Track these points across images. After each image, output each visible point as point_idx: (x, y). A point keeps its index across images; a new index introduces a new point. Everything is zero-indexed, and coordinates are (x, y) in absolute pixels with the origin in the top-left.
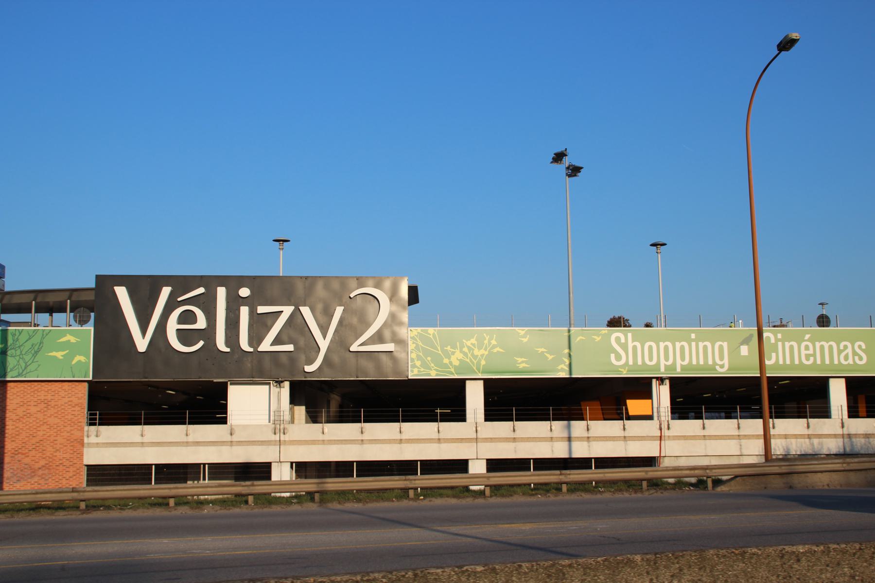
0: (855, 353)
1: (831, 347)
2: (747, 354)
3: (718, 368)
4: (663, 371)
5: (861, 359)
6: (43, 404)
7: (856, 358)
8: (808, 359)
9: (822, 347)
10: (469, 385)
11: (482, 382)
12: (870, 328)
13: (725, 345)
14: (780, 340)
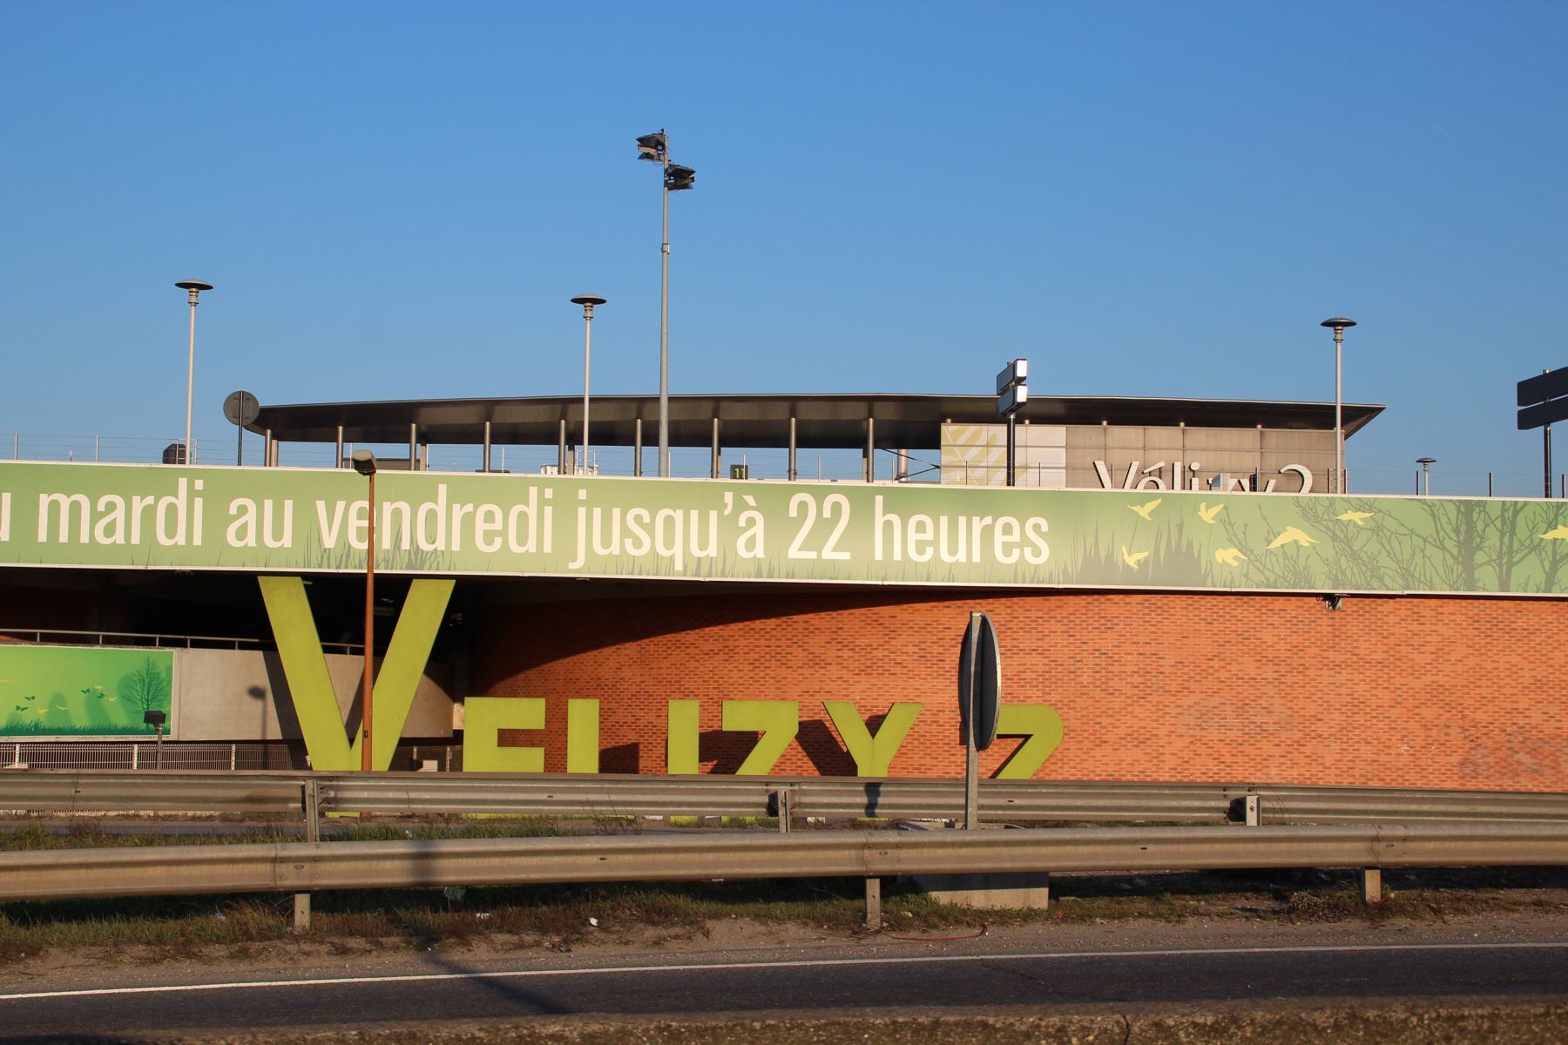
0: (626, 532)
1: (75, 508)
6: (716, 649)
7: (628, 542)
8: (920, 551)
12: (635, 478)
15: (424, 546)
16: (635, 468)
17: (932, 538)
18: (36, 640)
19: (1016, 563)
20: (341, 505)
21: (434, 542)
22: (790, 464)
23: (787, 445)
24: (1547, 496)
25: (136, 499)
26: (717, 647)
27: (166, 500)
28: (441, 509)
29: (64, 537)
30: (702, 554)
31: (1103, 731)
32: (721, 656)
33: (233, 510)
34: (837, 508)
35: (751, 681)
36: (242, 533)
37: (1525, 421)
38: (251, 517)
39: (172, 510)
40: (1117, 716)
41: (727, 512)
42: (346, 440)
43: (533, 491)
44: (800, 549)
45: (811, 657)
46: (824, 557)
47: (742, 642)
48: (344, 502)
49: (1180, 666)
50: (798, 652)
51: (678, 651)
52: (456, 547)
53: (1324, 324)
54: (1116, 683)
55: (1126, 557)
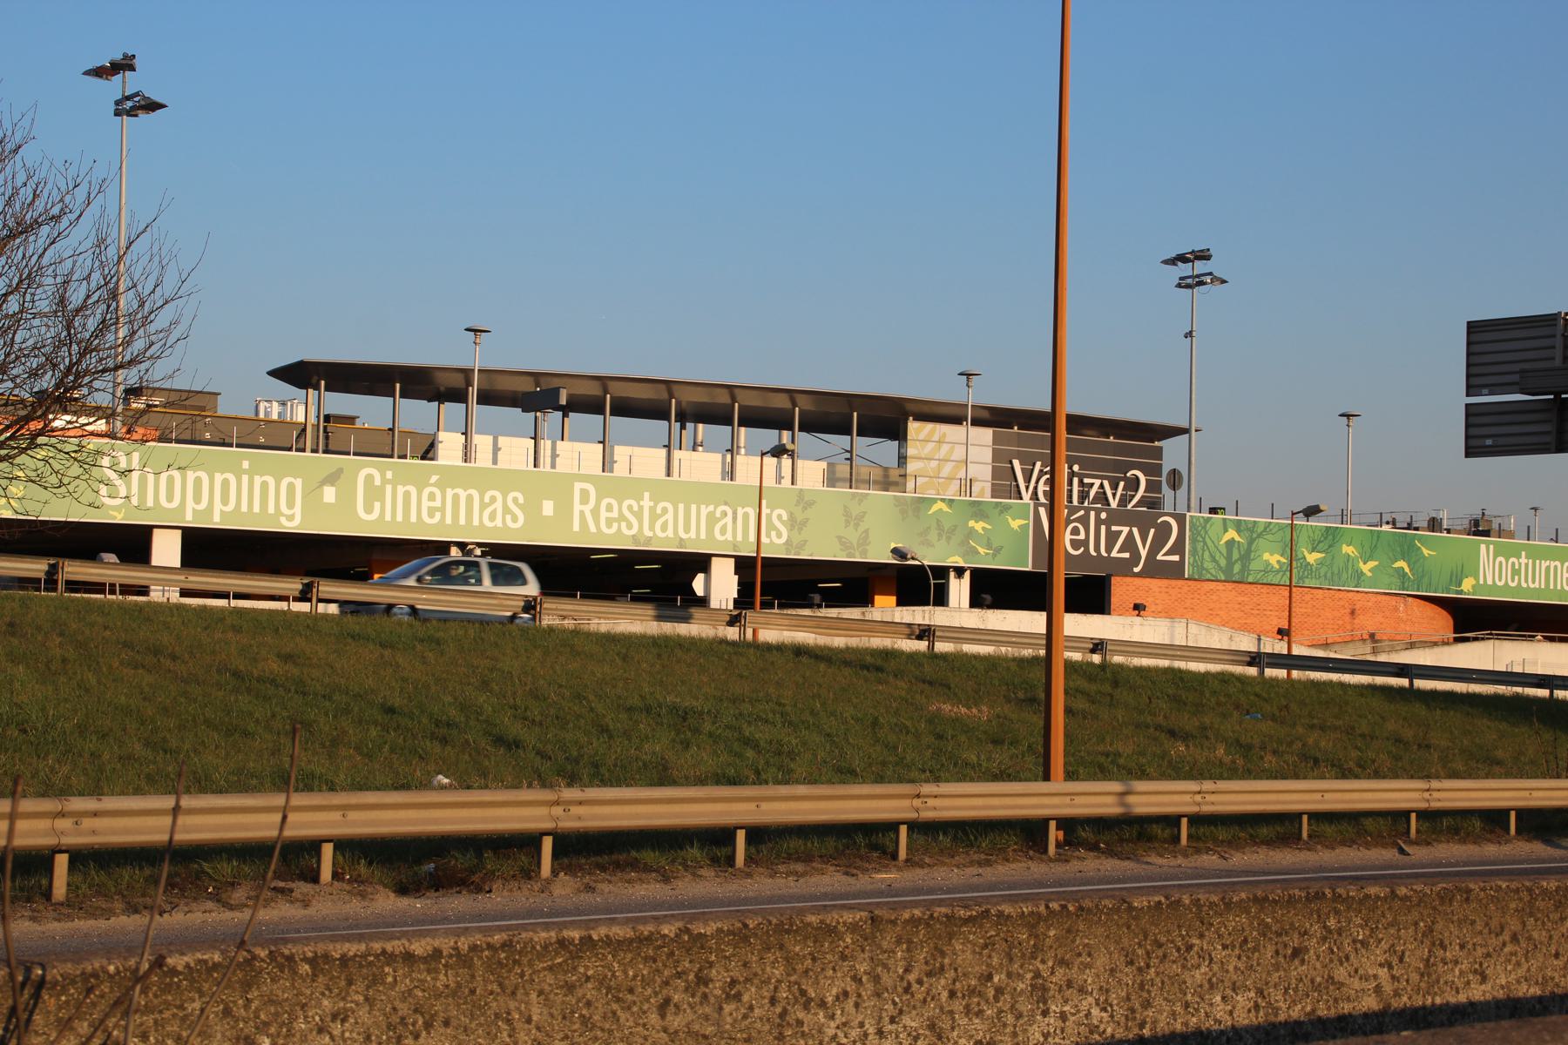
0: (506, 510)
1: (470, 498)
2: (325, 501)
3: (283, 520)
4: (191, 519)
5: (515, 519)
8: (431, 515)
9: (456, 498)
10: (158, 536)
11: (180, 532)
13: (298, 483)
14: (389, 482)
38: (670, 516)
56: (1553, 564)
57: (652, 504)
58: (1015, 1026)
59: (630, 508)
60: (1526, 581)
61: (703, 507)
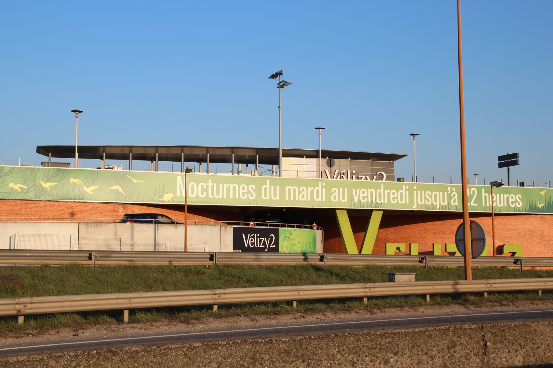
0: (426, 198)
1: (294, 190)
12: (434, 184)
15: (379, 202)
16: (518, 184)
17: (396, 197)
18: (302, 228)
19: (515, 207)
20: (358, 190)
21: (422, 202)
22: (207, 168)
23: (129, 159)
24: (509, 186)
25: (309, 188)
26: (422, 229)
27: (317, 188)
28: (382, 191)
29: (292, 199)
30: (443, 204)
31: (532, 251)
32: (424, 232)
33: (332, 191)
34: (474, 191)
35: (433, 238)
36: (335, 198)
37: (501, 165)
38: (337, 193)
39: (318, 191)
40: (535, 247)
41: (449, 193)
42: (52, 156)
43: (320, 183)
44: (473, 203)
45: (452, 232)
46: (471, 205)
47: (430, 228)
48: (359, 189)
49: (549, 234)
50: (447, 230)
51: (408, 230)
52: (386, 202)
53: (410, 135)
54: (534, 238)
55: (539, 205)
56: (232, 186)
57: (212, 184)
58: (398, 348)
59: (428, 194)
60: (212, 194)
61: (225, 185)
